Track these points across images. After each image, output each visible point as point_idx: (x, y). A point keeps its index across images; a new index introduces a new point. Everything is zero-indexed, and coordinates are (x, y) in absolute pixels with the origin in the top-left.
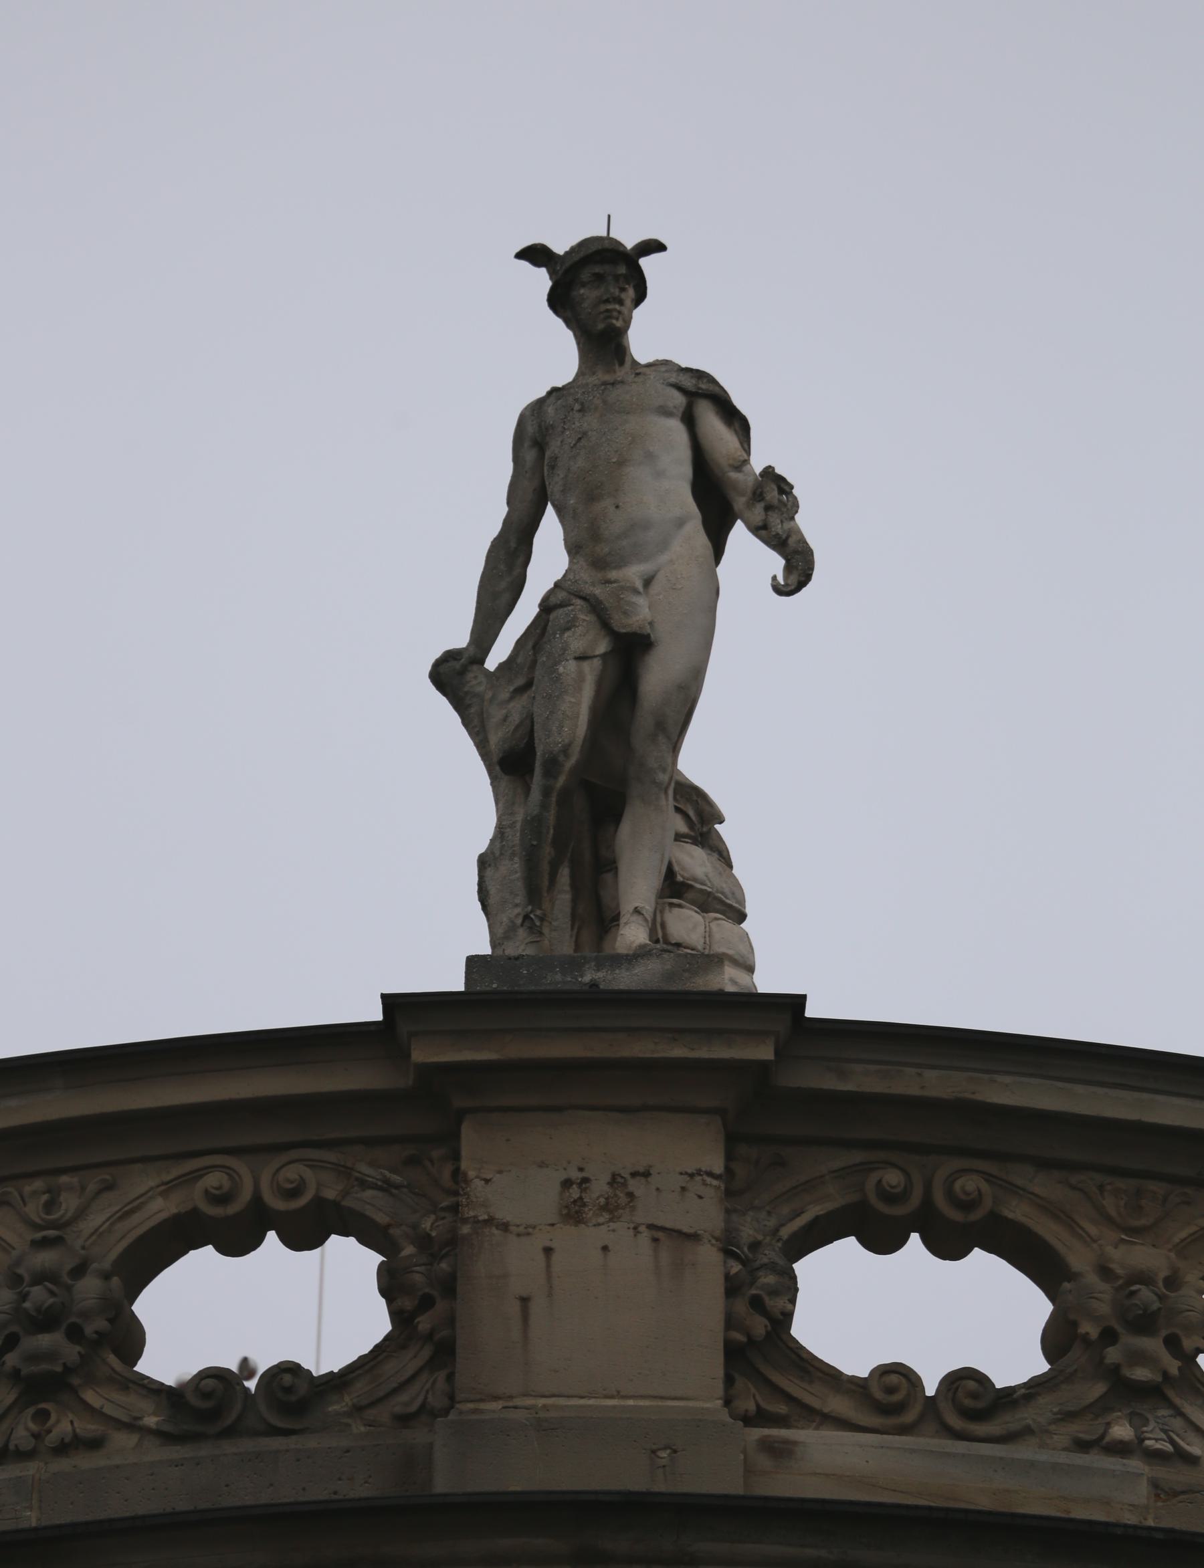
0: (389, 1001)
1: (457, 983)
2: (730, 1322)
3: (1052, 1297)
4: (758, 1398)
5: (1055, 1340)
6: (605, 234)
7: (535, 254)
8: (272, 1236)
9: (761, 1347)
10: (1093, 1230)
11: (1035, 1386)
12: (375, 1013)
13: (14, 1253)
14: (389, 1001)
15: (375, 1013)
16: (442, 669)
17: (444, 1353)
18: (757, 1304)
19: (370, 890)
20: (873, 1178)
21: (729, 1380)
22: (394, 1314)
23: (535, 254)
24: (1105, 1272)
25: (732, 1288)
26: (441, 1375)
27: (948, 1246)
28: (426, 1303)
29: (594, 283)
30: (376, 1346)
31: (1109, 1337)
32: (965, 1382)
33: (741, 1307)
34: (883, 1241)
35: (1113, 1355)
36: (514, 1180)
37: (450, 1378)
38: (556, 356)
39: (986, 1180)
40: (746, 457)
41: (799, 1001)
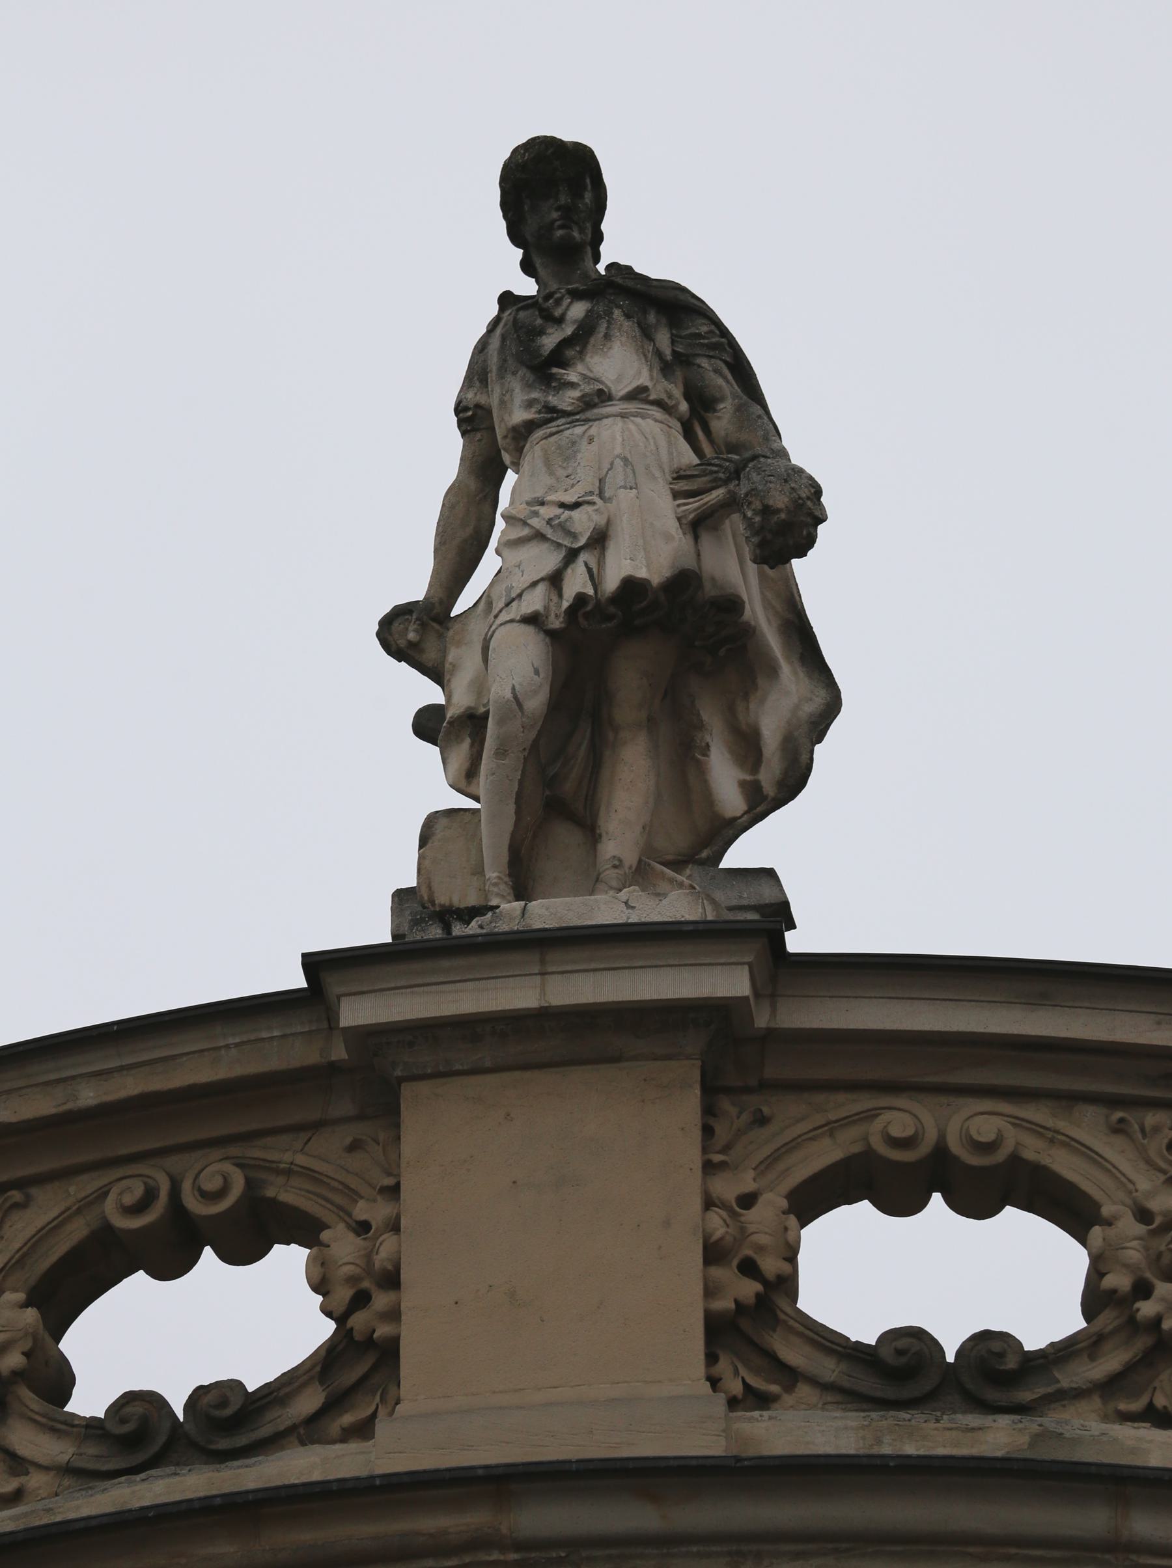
0: (313, 963)
1: (382, 934)
2: (710, 1292)
4: (743, 1372)
8: (208, 1251)
9: (754, 1323)
10: (676, 1550)
12: (299, 981)
14: (313, 963)
15: (299, 981)
16: (394, 648)
18: (749, 1268)
19: (273, 828)
20: (878, 1124)
21: (711, 1358)
24: (1143, 1215)
25: (713, 1253)
28: (361, 1300)
29: (551, 191)
31: (1143, 1290)
32: (989, 1347)
35: (1147, 1309)
36: (462, 1156)
38: (505, 270)
39: (1013, 1124)
40: (786, 1268)
41: (792, 926)
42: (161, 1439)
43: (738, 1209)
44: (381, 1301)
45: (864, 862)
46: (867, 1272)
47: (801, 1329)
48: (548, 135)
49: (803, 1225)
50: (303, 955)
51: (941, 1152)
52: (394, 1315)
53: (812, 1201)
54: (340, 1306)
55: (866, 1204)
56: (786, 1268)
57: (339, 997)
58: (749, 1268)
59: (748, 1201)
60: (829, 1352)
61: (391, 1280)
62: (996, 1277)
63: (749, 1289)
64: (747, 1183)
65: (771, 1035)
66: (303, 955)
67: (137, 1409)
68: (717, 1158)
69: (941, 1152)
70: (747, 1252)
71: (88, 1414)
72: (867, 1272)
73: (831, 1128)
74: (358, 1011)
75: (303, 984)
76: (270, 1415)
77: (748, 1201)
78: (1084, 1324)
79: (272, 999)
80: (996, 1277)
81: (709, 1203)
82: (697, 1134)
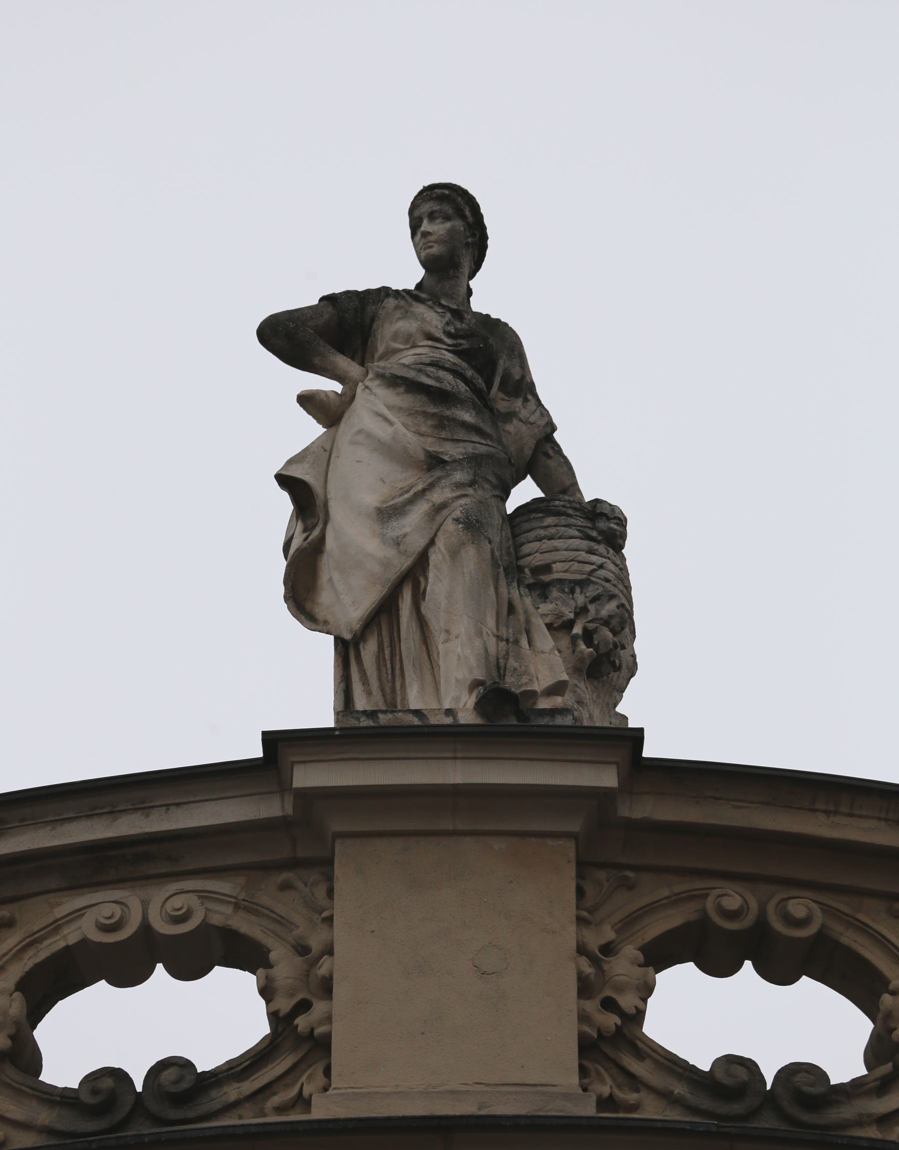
0: (271, 739)
2: (583, 1017)
3: (873, 1020)
5: (875, 1053)
6: (570, 848)
7: (451, 225)
9: (614, 1039)
11: (856, 1083)
12: (256, 751)
13: (370, 376)
14: (271, 739)
15: (256, 751)
17: (319, 1047)
18: (609, 1005)
21: (583, 1071)
22: (273, 1016)
23: (451, 225)
25: (585, 988)
26: (319, 1068)
27: (779, 972)
30: (482, 216)
33: (592, 1006)
34: (720, 966)
37: (327, 1072)
40: (640, 1004)
42: (127, 1109)
43: (600, 956)
44: (319, 1008)
45: (690, 701)
46: (699, 1015)
47: (29, 1090)
48: (478, 200)
49: (657, 971)
50: (264, 733)
51: (761, 925)
52: (328, 1019)
53: (661, 955)
54: (284, 1005)
55: (103, 983)
56: (640, 1004)
57: (293, 763)
58: (609, 1005)
59: (608, 949)
60: (680, 1077)
61: (326, 988)
62: (808, 1028)
63: (611, 1021)
64: (609, 935)
65: (632, 825)
66: (264, 733)
67: (108, 1083)
68: (585, 914)
69: (761, 925)
70: (608, 993)
71: (61, 1084)
72: (699, 1015)
73: (676, 901)
74: (308, 776)
75: (646, 753)
76: (214, 1093)
77: (608, 949)
78: (865, 1072)
79: (666, 764)
80: (808, 1028)
81: (582, 950)
82: (572, 896)
